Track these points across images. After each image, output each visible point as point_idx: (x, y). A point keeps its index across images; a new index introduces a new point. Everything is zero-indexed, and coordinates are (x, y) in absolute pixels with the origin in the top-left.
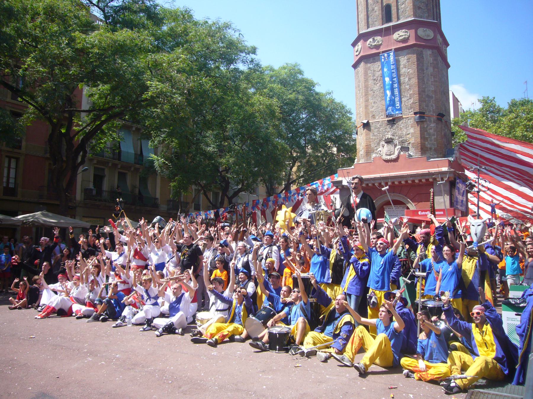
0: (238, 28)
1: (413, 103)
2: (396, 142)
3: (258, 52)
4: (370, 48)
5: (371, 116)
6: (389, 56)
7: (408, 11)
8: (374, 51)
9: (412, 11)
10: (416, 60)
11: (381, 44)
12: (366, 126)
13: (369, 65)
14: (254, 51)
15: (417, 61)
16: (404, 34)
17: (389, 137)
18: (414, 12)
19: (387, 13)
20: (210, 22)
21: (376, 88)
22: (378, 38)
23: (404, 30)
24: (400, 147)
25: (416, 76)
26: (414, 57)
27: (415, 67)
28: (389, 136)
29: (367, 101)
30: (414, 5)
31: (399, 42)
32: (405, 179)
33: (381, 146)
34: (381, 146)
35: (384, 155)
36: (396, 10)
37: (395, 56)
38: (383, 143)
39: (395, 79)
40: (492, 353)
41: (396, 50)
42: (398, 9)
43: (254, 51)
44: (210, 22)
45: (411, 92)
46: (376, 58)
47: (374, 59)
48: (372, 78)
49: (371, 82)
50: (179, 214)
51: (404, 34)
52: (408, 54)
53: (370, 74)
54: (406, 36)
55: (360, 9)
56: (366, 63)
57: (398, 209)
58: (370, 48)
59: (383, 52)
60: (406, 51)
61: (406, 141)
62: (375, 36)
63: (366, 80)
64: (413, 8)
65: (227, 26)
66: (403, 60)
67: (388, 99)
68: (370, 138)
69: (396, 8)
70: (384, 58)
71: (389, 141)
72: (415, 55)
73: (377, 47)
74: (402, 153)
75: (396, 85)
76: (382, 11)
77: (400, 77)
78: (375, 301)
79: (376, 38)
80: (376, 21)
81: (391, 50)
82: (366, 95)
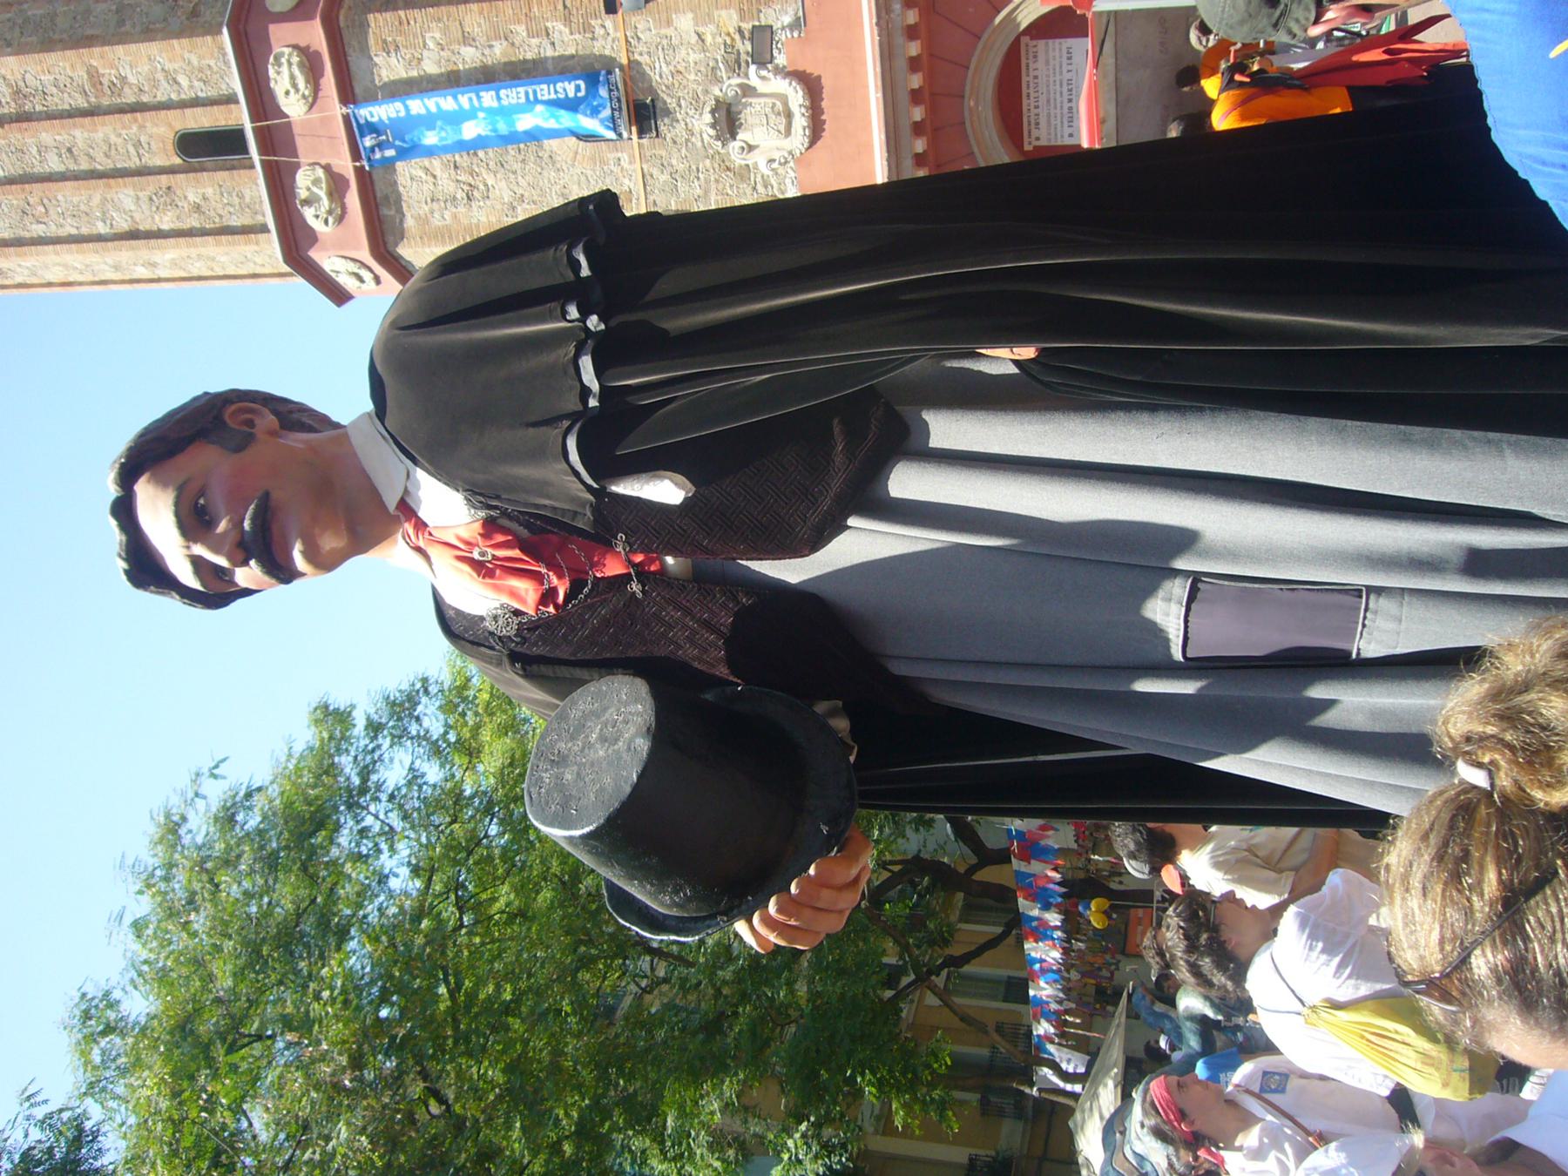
0: (184, 781)
1: (567, 20)
2: (729, 86)
3: (339, 701)
4: (340, 219)
6: (372, 128)
7: (201, 58)
8: (353, 199)
9: (199, 40)
10: (388, 15)
11: (327, 168)
13: (409, 222)
14: (334, 718)
15: (396, 9)
16: (285, 69)
17: (708, 118)
18: (204, 34)
19: (209, 148)
20: (144, 906)
22: (304, 181)
23: (272, 72)
24: (753, 68)
25: (453, 9)
26: (380, 24)
28: (703, 122)
30: (179, 35)
31: (316, 89)
32: (899, 39)
33: (752, 159)
34: (752, 159)
35: (788, 144)
36: (199, 110)
37: (372, 98)
38: (735, 146)
41: (348, 94)
42: (196, 103)
43: (334, 718)
44: (144, 906)
45: (521, 30)
46: (380, 188)
47: (386, 198)
48: (462, 209)
50: (1035, 1092)
51: (285, 69)
52: (364, 49)
53: (447, 215)
54: (295, 59)
55: (198, 268)
56: (401, 235)
57: (1042, 81)
58: (340, 219)
59: (356, 154)
60: (354, 59)
61: (729, 48)
62: (294, 195)
64: (191, 36)
65: (172, 829)
66: (390, 68)
69: (188, 111)
70: (381, 146)
71: (728, 120)
72: (371, 17)
73: (337, 186)
74: (781, 60)
76: (203, 170)
79: (303, 194)
80: (241, 196)
81: (346, 119)
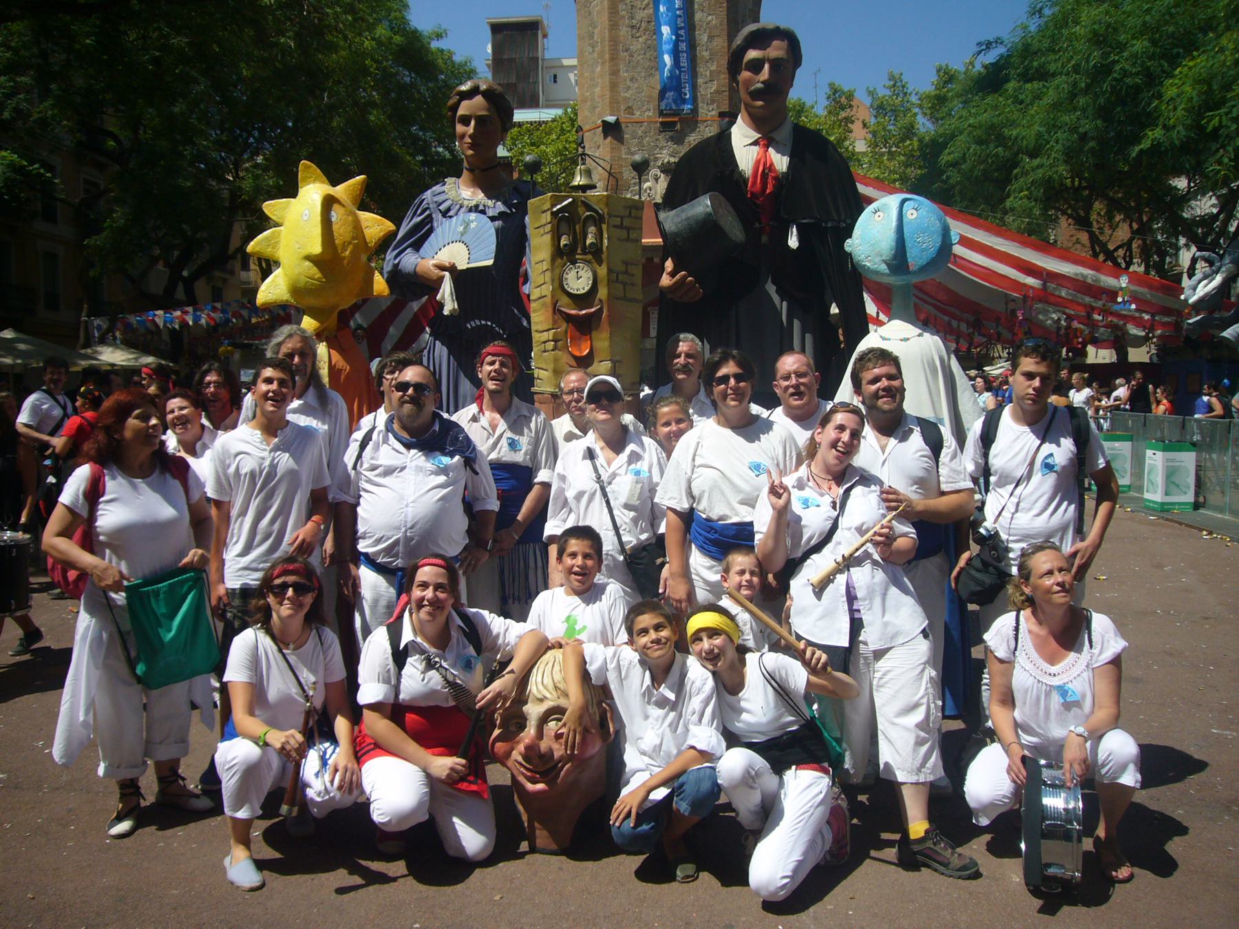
1: (717, 92)
5: (623, 108)
12: (612, 130)
21: (637, 45)
25: (725, 33)
27: (723, 12)
29: (615, 73)
39: (682, 32)
40: (425, 579)
45: (714, 68)
48: (627, 22)
49: (624, 31)
63: (614, 26)
67: (666, 73)
68: (620, 158)
75: (683, 46)
77: (694, 30)
78: (834, 486)
82: (614, 58)
